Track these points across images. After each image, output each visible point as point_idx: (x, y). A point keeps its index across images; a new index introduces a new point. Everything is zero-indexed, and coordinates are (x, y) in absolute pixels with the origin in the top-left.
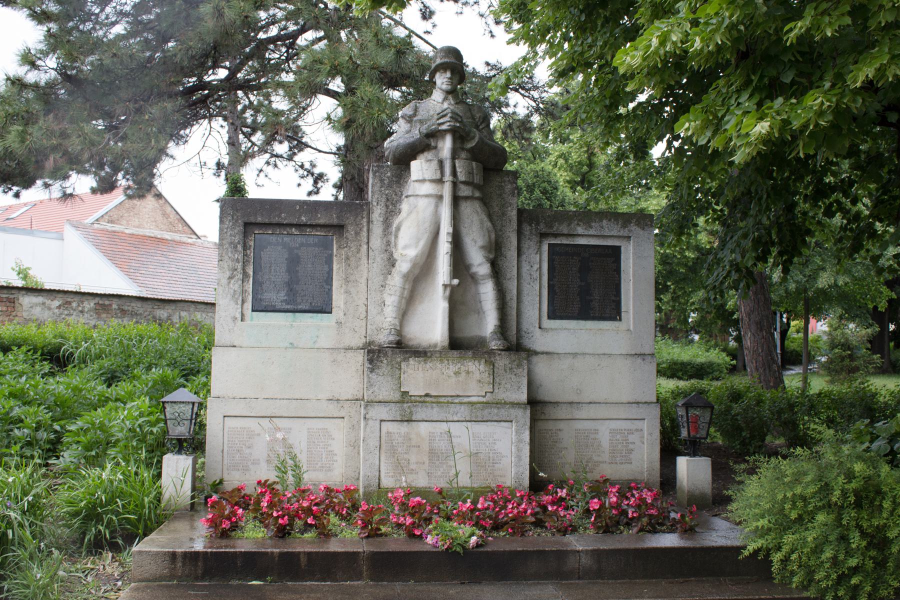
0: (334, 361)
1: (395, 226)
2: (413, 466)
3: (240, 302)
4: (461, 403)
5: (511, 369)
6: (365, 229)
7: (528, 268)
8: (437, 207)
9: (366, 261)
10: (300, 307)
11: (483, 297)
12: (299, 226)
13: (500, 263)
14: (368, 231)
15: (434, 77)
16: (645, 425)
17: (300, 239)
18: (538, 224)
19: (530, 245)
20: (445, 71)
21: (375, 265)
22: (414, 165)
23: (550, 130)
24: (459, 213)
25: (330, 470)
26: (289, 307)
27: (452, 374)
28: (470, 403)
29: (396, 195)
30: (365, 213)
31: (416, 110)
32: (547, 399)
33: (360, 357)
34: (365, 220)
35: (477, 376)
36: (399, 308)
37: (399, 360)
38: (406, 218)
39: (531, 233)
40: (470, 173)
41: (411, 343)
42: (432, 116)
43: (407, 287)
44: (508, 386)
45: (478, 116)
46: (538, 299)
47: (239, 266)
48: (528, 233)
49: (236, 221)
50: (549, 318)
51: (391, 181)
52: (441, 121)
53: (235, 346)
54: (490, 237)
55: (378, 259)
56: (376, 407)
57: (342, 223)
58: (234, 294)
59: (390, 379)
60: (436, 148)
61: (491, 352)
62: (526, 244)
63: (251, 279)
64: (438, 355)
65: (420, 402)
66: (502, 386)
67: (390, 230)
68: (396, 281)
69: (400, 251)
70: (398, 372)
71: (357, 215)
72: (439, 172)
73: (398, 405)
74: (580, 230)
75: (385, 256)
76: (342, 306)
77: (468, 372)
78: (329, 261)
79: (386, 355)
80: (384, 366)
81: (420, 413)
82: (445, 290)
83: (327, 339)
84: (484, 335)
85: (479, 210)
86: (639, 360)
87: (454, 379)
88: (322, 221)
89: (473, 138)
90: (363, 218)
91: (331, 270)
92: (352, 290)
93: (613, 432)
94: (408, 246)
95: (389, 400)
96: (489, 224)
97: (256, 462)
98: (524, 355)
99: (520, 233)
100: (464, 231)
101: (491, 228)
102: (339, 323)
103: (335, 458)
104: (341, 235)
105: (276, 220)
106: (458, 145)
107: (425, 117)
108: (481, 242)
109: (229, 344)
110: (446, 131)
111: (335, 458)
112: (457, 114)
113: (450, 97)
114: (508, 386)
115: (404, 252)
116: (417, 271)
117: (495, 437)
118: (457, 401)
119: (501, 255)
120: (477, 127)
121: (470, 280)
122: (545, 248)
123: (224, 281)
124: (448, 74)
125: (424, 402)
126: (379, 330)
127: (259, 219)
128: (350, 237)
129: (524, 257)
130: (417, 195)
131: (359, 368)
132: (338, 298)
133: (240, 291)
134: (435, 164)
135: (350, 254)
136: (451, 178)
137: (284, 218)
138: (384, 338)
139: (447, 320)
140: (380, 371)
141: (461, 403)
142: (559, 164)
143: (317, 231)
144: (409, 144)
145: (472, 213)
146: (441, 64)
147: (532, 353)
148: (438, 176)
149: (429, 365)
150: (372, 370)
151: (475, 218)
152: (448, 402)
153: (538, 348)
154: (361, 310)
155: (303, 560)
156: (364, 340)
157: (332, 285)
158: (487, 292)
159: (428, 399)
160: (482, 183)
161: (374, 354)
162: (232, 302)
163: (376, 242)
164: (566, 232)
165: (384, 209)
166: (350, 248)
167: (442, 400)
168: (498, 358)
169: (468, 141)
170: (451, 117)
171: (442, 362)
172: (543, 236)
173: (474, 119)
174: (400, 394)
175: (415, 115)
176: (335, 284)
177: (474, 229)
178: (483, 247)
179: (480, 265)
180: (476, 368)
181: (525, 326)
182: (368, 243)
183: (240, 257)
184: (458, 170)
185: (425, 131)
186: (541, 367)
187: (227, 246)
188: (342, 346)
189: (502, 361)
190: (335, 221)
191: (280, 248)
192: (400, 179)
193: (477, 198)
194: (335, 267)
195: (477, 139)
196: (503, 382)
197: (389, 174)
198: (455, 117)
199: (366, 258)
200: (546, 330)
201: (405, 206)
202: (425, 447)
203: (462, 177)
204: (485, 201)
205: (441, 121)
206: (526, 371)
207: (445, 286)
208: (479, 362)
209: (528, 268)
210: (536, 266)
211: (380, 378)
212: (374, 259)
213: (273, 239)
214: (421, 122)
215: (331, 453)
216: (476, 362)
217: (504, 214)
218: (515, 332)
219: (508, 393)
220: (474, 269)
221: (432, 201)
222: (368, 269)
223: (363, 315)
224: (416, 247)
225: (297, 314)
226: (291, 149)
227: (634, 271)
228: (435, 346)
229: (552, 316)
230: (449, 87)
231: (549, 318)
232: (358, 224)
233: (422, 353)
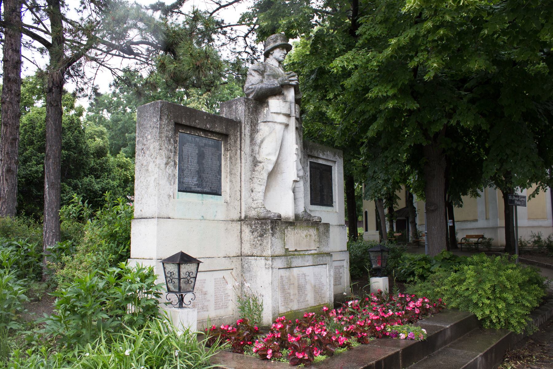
3: (172, 184)
6: (239, 139)
10: (205, 190)
12: (205, 131)
17: (204, 141)
25: (227, 307)
26: (199, 189)
28: (311, 254)
30: (239, 128)
34: (239, 133)
49: (170, 120)
52: (292, 78)
53: (169, 218)
56: (277, 260)
58: (169, 177)
63: (178, 166)
75: (251, 159)
81: (296, 262)
88: (218, 130)
91: (220, 166)
92: (233, 180)
104: (226, 142)
105: (193, 124)
122: (309, 163)
123: (163, 166)
132: (225, 186)
137: (197, 123)
143: (214, 136)
144: (270, 88)
159: (296, 253)
162: (168, 184)
163: (246, 148)
167: (301, 253)
187: (164, 138)
188: (229, 219)
190: (224, 131)
191: (193, 145)
194: (223, 163)
197: (252, 105)
202: (296, 284)
213: (189, 138)
215: (227, 295)
221: (283, 127)
223: (239, 198)
225: (204, 195)
227: (338, 180)
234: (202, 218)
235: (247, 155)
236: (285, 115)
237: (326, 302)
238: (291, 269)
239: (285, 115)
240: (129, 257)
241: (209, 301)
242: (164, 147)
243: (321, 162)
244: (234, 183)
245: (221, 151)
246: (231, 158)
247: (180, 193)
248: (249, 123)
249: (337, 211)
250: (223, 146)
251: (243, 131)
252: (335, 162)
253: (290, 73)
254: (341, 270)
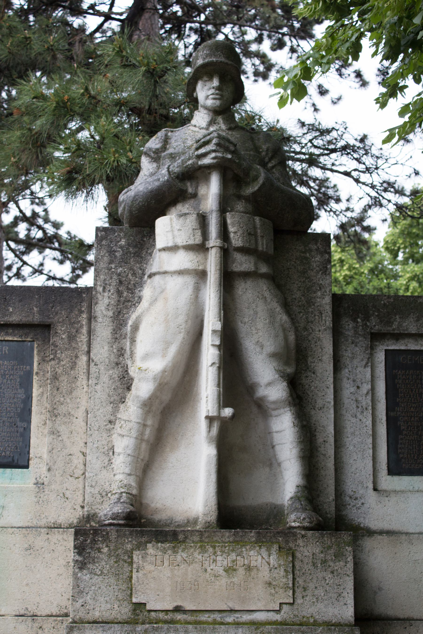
0: (30, 548)
1: (130, 323)
4: (237, 624)
5: (324, 562)
6: (84, 330)
7: (352, 390)
8: (197, 290)
9: (85, 382)
11: (277, 438)
13: (304, 381)
14: (89, 332)
15: (194, 90)
18: (367, 318)
19: (355, 354)
20: (211, 79)
21: (98, 387)
22: (162, 224)
23: (399, 248)
24: (233, 300)
27: (221, 572)
28: (253, 623)
29: (134, 274)
30: (85, 305)
31: (166, 141)
32: (391, 613)
33: (68, 540)
34: (84, 316)
35: (265, 574)
36: (135, 457)
37: (129, 547)
38: (148, 309)
39: (356, 332)
40: (251, 234)
41: (157, 517)
42: (189, 148)
43: (149, 422)
44: (320, 592)
45: (264, 147)
46: (370, 440)
48: (350, 333)
50: (391, 472)
51: (126, 253)
52: (202, 151)
54: (286, 339)
55: (105, 378)
57: (48, 321)
59: (112, 580)
60: (195, 196)
61: (289, 533)
62: (348, 352)
64: (196, 538)
65: (166, 622)
66: (309, 593)
67: (124, 331)
68: (131, 412)
69: (139, 363)
70: (126, 568)
71: (71, 309)
72: (199, 233)
73: (127, 627)
75: (116, 373)
76: (45, 456)
77: (249, 568)
78: (26, 384)
79: (106, 538)
80: (104, 559)
82: (210, 426)
83: (17, 514)
84: (279, 502)
85: (267, 294)
87: (224, 581)
88: (15, 319)
89: (256, 178)
90: (81, 312)
91: (29, 398)
92: (62, 429)
94: (152, 355)
95: (111, 617)
96: (285, 318)
98: (346, 536)
99: (337, 334)
100: (243, 329)
101: (288, 325)
102: (39, 485)
104: (46, 340)
106: (231, 191)
107: (180, 149)
108: (270, 347)
110: (209, 168)
112: (228, 141)
113: (220, 119)
114: (320, 592)
115: (144, 366)
116: (166, 397)
118: (230, 619)
119: (307, 368)
120: (264, 165)
121: (255, 410)
122: (380, 357)
124: (216, 82)
125: (172, 622)
126: (104, 495)
128: (59, 343)
129: (345, 372)
130: (165, 273)
132: (39, 443)
134: (191, 221)
135: (59, 371)
136: (218, 243)
138: (109, 509)
139: (213, 477)
140: (96, 568)
141: (237, 624)
142: (411, 288)
143: (7, 334)
144: (151, 191)
145: (257, 306)
146: (203, 66)
147: (359, 533)
148: (198, 239)
149: (181, 555)
150: (81, 565)
151: (261, 309)
152: (215, 622)
153: (374, 524)
154: (75, 461)
156: (79, 513)
157: (29, 422)
158: (284, 428)
159: (179, 616)
160: (271, 251)
161: (88, 536)
163: (102, 351)
165: (115, 296)
166: (60, 360)
167: (204, 617)
168: (300, 542)
169: (247, 184)
170: (217, 145)
171: (203, 550)
172: (376, 337)
173: (260, 153)
174: (130, 607)
175: (164, 148)
176: (36, 419)
177: (260, 325)
178: (274, 356)
179: (269, 384)
180: (263, 561)
181: (350, 486)
182: (89, 352)
184: (231, 229)
185: (176, 170)
186: (380, 558)
188: (43, 523)
189: (309, 548)
190: (37, 318)
192: (141, 249)
193: (263, 276)
194: (36, 392)
195: (261, 180)
196: (311, 586)
197: (123, 242)
198: (223, 144)
199: (85, 377)
200: (386, 493)
201: (147, 292)
203: (236, 240)
204: (278, 282)
205: (202, 151)
206: (350, 565)
207: (210, 419)
208: (269, 550)
209: (352, 390)
210: (366, 387)
211: (96, 580)
212: (98, 378)
214: (172, 157)
216: (264, 551)
217: (310, 302)
218: (332, 497)
219: (320, 606)
220: (261, 392)
222: (89, 394)
224: (164, 356)
226: (74, 270)
228: (195, 521)
229: (394, 470)
230: (218, 103)
231: (391, 472)
232: (74, 324)
233: (169, 534)
236: (189, 248)
239: (189, 248)
244: (64, 437)
245: (32, 365)
250: (35, 352)
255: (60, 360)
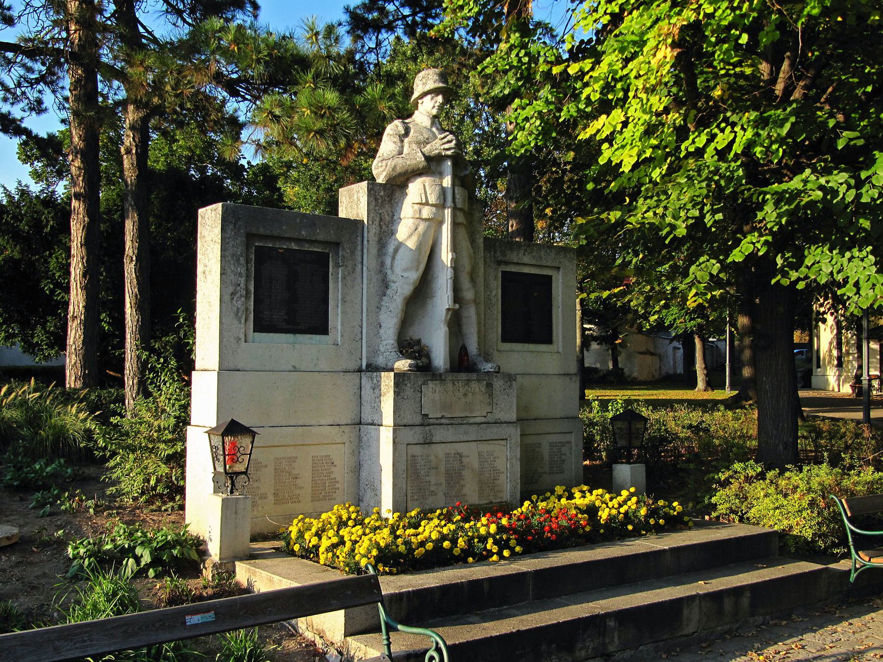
2: (432, 488)
3: (243, 321)
6: (359, 248)
16: (572, 438)
47: (242, 280)
58: (238, 312)
65: (437, 424)
70: (419, 395)
74: (526, 259)
82: (447, 314)
86: (568, 378)
87: (463, 400)
88: (321, 237)
93: (552, 445)
97: (264, 497)
103: (337, 485)
105: (276, 233)
109: (232, 367)
110: (447, 156)
111: (337, 485)
117: (495, 455)
127: (262, 231)
131: (356, 390)
132: (336, 318)
133: (243, 308)
143: (315, 247)
155: (486, 586)
159: (443, 421)
162: (236, 322)
164: (515, 261)
166: (347, 266)
172: (499, 263)
183: (243, 271)
184: (457, 196)
187: (230, 258)
190: (332, 238)
202: (442, 469)
234: (293, 369)
235: (372, 273)
237: (505, 499)
238: (433, 446)
240: (189, 424)
241: (302, 488)
242: (229, 270)
243: (526, 270)
246: (344, 278)
247: (256, 334)
248: (377, 223)
249: (561, 350)
251: (365, 235)
252: (558, 268)
253: (445, 137)
254: (564, 450)
255: (347, 266)
